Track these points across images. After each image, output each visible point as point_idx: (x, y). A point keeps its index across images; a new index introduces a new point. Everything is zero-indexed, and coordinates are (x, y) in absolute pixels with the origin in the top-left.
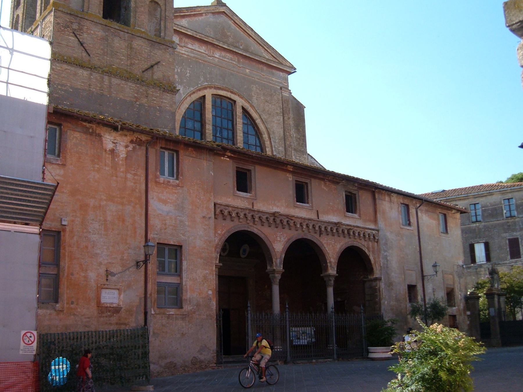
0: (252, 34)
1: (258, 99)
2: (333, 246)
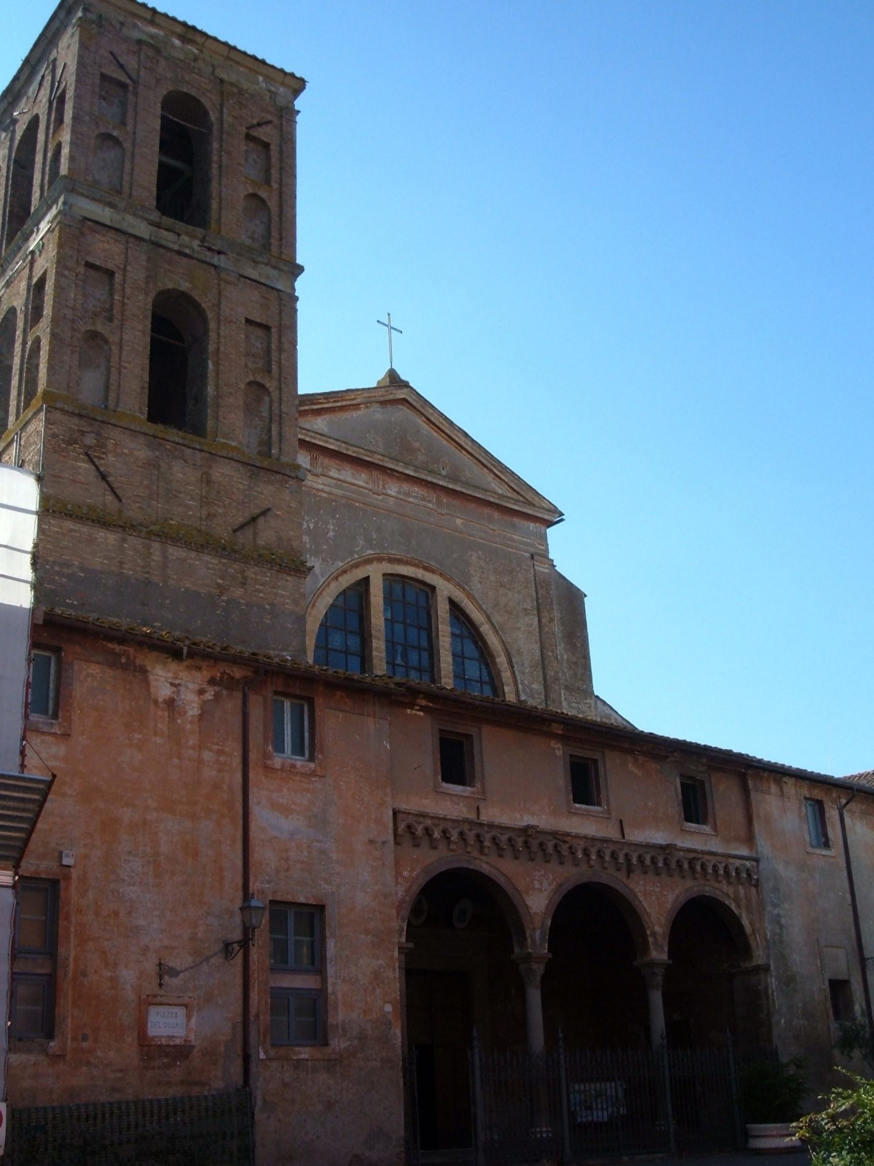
0: (467, 444)
1: (482, 580)
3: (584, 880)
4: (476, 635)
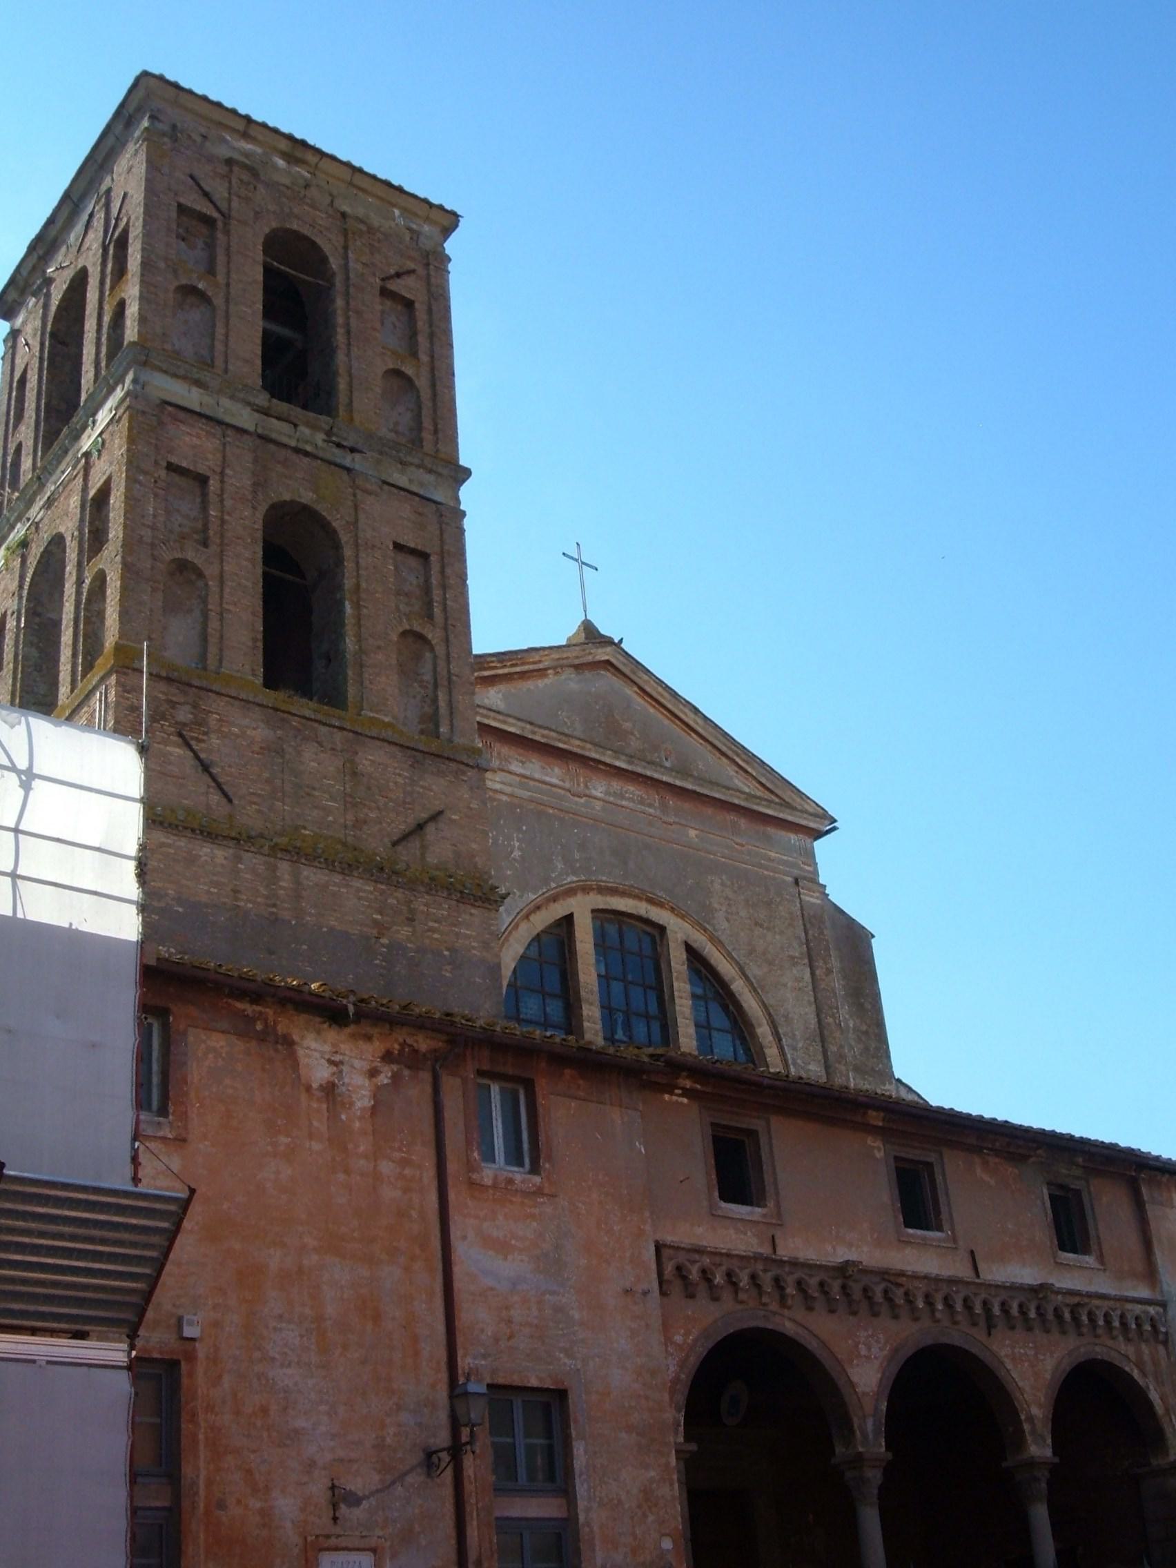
0: (697, 724)
1: (729, 916)
4: (725, 996)
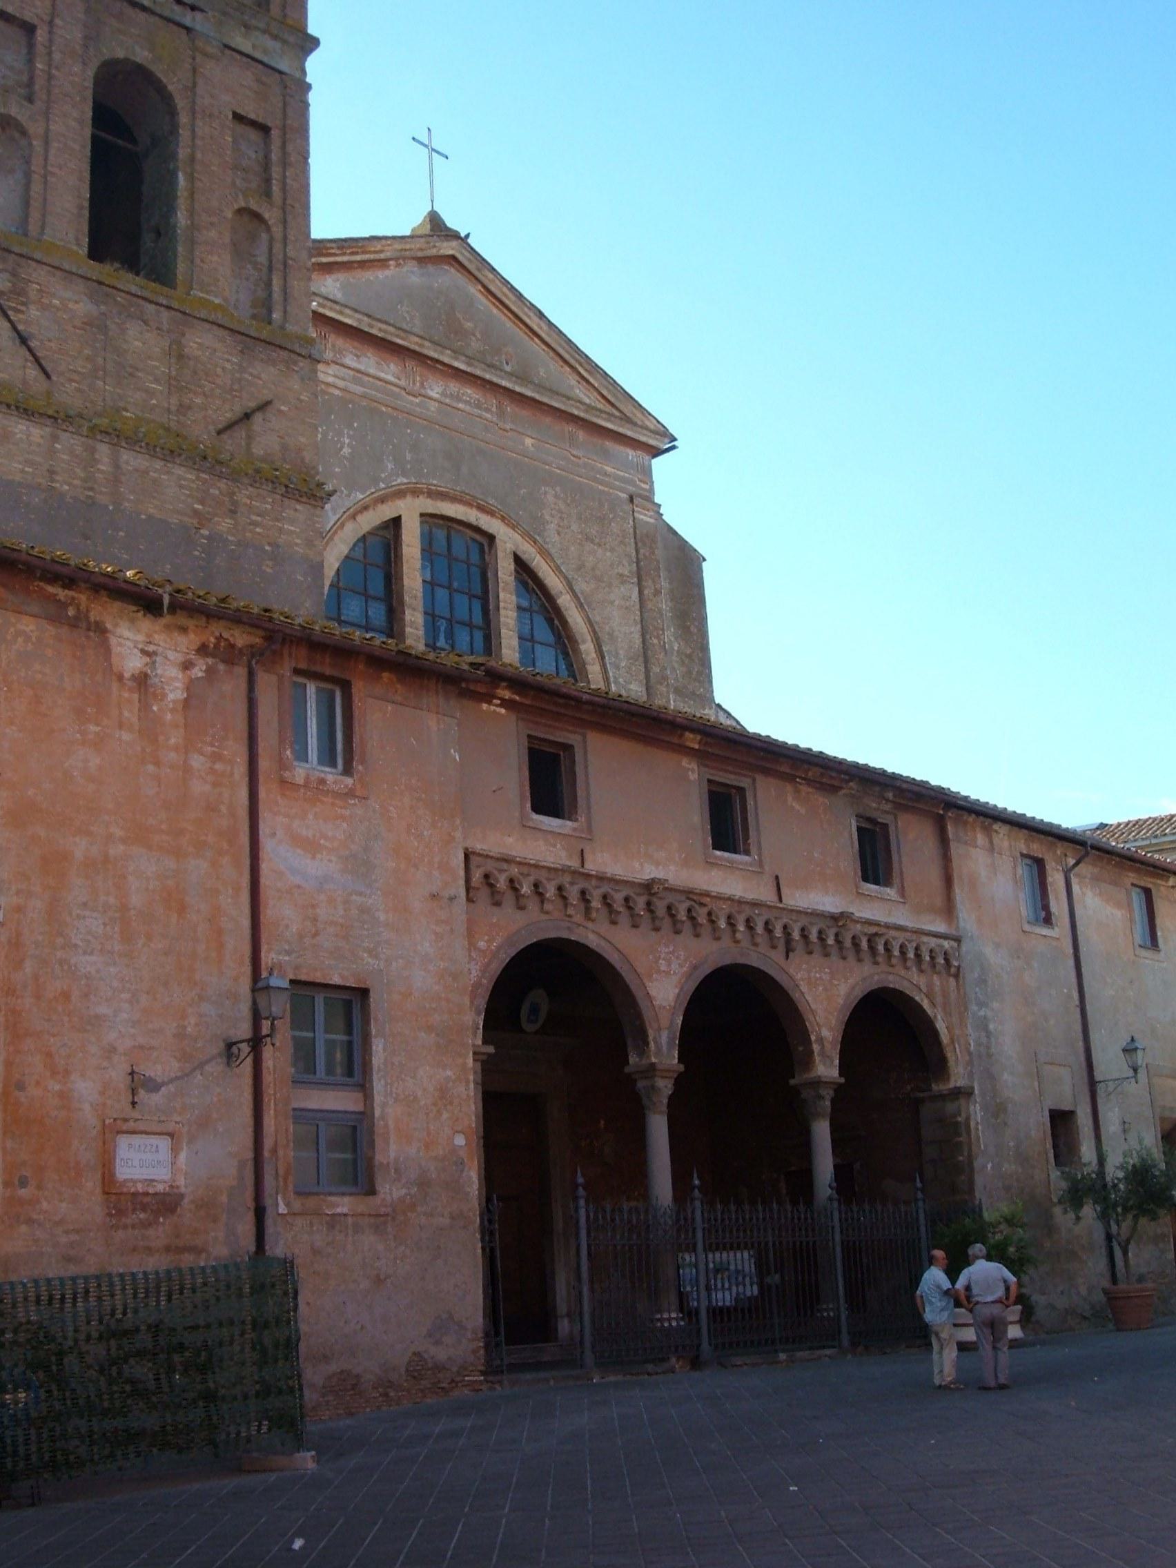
0: (541, 328)
1: (560, 529)
2: (825, 989)
3: (727, 961)
